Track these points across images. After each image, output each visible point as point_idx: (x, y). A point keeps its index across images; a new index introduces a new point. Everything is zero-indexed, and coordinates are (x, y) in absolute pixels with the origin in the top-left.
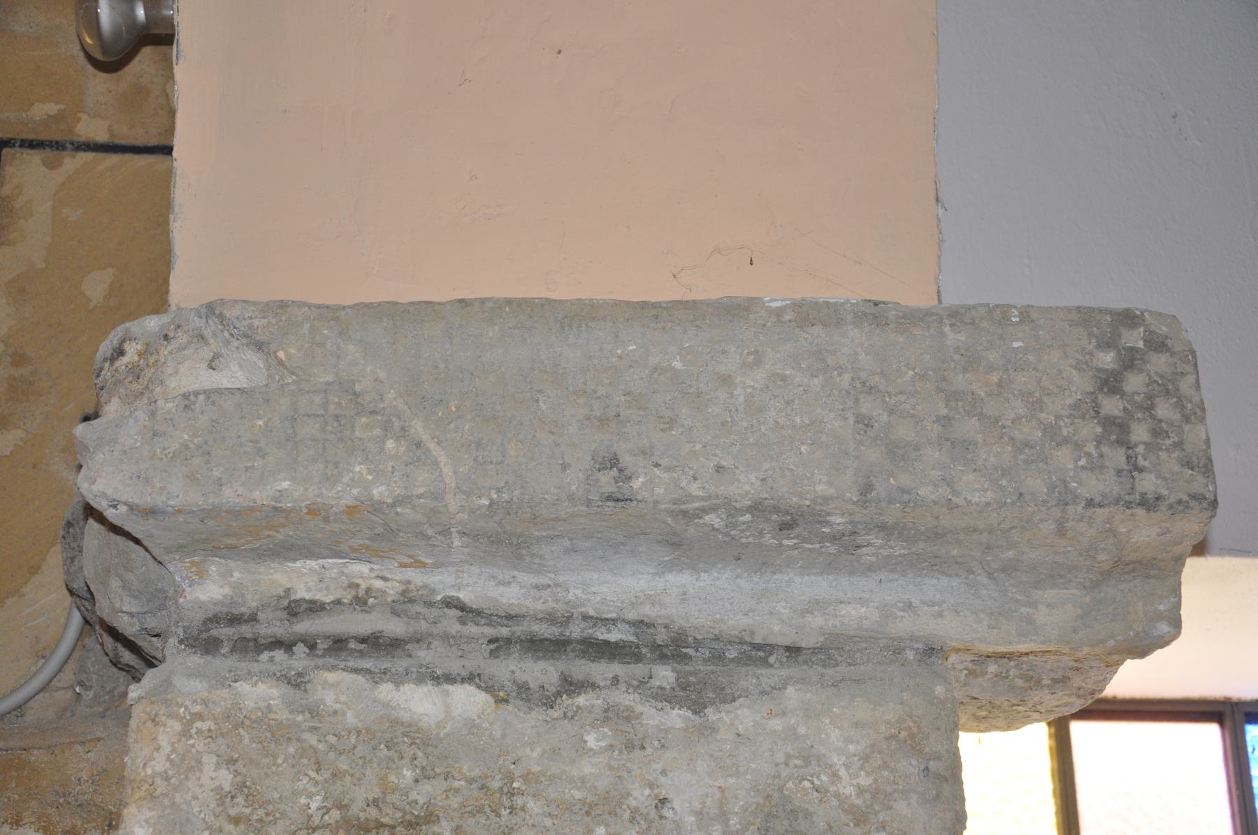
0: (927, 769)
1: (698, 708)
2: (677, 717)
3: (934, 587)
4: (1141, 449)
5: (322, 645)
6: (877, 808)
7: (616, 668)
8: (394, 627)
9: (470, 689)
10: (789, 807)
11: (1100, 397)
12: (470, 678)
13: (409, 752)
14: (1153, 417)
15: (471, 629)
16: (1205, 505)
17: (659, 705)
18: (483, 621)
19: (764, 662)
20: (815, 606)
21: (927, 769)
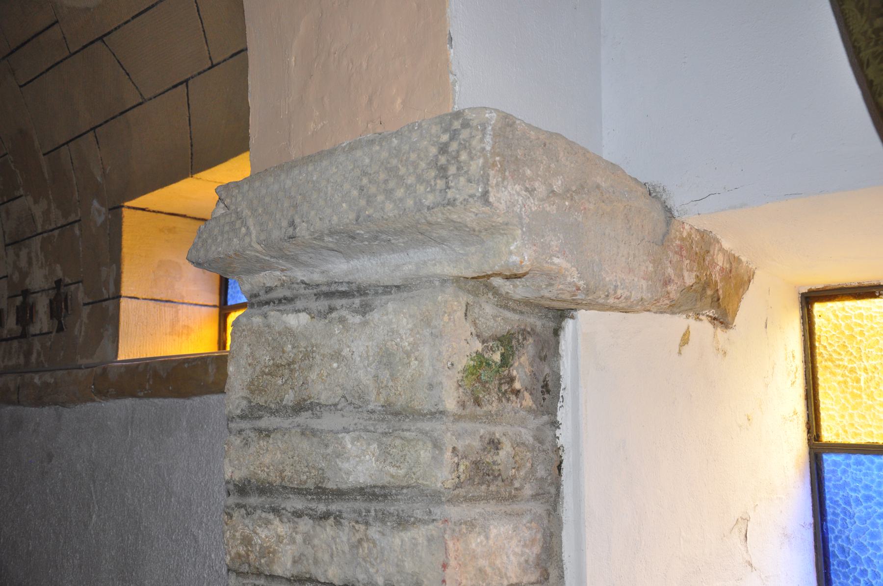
0: (432, 333)
1: (364, 314)
2: (358, 319)
3: (433, 252)
4: (451, 178)
5: (277, 302)
6: (413, 351)
7: (344, 301)
8: (288, 294)
9: (304, 314)
10: (388, 353)
11: (440, 157)
12: (304, 310)
13: (290, 338)
14: (458, 161)
15: (307, 291)
16: (475, 199)
17: (354, 314)
18: (311, 288)
19: (390, 293)
20: (398, 267)
21: (432, 333)
